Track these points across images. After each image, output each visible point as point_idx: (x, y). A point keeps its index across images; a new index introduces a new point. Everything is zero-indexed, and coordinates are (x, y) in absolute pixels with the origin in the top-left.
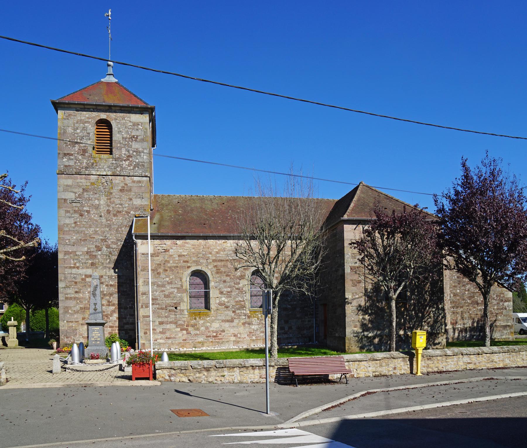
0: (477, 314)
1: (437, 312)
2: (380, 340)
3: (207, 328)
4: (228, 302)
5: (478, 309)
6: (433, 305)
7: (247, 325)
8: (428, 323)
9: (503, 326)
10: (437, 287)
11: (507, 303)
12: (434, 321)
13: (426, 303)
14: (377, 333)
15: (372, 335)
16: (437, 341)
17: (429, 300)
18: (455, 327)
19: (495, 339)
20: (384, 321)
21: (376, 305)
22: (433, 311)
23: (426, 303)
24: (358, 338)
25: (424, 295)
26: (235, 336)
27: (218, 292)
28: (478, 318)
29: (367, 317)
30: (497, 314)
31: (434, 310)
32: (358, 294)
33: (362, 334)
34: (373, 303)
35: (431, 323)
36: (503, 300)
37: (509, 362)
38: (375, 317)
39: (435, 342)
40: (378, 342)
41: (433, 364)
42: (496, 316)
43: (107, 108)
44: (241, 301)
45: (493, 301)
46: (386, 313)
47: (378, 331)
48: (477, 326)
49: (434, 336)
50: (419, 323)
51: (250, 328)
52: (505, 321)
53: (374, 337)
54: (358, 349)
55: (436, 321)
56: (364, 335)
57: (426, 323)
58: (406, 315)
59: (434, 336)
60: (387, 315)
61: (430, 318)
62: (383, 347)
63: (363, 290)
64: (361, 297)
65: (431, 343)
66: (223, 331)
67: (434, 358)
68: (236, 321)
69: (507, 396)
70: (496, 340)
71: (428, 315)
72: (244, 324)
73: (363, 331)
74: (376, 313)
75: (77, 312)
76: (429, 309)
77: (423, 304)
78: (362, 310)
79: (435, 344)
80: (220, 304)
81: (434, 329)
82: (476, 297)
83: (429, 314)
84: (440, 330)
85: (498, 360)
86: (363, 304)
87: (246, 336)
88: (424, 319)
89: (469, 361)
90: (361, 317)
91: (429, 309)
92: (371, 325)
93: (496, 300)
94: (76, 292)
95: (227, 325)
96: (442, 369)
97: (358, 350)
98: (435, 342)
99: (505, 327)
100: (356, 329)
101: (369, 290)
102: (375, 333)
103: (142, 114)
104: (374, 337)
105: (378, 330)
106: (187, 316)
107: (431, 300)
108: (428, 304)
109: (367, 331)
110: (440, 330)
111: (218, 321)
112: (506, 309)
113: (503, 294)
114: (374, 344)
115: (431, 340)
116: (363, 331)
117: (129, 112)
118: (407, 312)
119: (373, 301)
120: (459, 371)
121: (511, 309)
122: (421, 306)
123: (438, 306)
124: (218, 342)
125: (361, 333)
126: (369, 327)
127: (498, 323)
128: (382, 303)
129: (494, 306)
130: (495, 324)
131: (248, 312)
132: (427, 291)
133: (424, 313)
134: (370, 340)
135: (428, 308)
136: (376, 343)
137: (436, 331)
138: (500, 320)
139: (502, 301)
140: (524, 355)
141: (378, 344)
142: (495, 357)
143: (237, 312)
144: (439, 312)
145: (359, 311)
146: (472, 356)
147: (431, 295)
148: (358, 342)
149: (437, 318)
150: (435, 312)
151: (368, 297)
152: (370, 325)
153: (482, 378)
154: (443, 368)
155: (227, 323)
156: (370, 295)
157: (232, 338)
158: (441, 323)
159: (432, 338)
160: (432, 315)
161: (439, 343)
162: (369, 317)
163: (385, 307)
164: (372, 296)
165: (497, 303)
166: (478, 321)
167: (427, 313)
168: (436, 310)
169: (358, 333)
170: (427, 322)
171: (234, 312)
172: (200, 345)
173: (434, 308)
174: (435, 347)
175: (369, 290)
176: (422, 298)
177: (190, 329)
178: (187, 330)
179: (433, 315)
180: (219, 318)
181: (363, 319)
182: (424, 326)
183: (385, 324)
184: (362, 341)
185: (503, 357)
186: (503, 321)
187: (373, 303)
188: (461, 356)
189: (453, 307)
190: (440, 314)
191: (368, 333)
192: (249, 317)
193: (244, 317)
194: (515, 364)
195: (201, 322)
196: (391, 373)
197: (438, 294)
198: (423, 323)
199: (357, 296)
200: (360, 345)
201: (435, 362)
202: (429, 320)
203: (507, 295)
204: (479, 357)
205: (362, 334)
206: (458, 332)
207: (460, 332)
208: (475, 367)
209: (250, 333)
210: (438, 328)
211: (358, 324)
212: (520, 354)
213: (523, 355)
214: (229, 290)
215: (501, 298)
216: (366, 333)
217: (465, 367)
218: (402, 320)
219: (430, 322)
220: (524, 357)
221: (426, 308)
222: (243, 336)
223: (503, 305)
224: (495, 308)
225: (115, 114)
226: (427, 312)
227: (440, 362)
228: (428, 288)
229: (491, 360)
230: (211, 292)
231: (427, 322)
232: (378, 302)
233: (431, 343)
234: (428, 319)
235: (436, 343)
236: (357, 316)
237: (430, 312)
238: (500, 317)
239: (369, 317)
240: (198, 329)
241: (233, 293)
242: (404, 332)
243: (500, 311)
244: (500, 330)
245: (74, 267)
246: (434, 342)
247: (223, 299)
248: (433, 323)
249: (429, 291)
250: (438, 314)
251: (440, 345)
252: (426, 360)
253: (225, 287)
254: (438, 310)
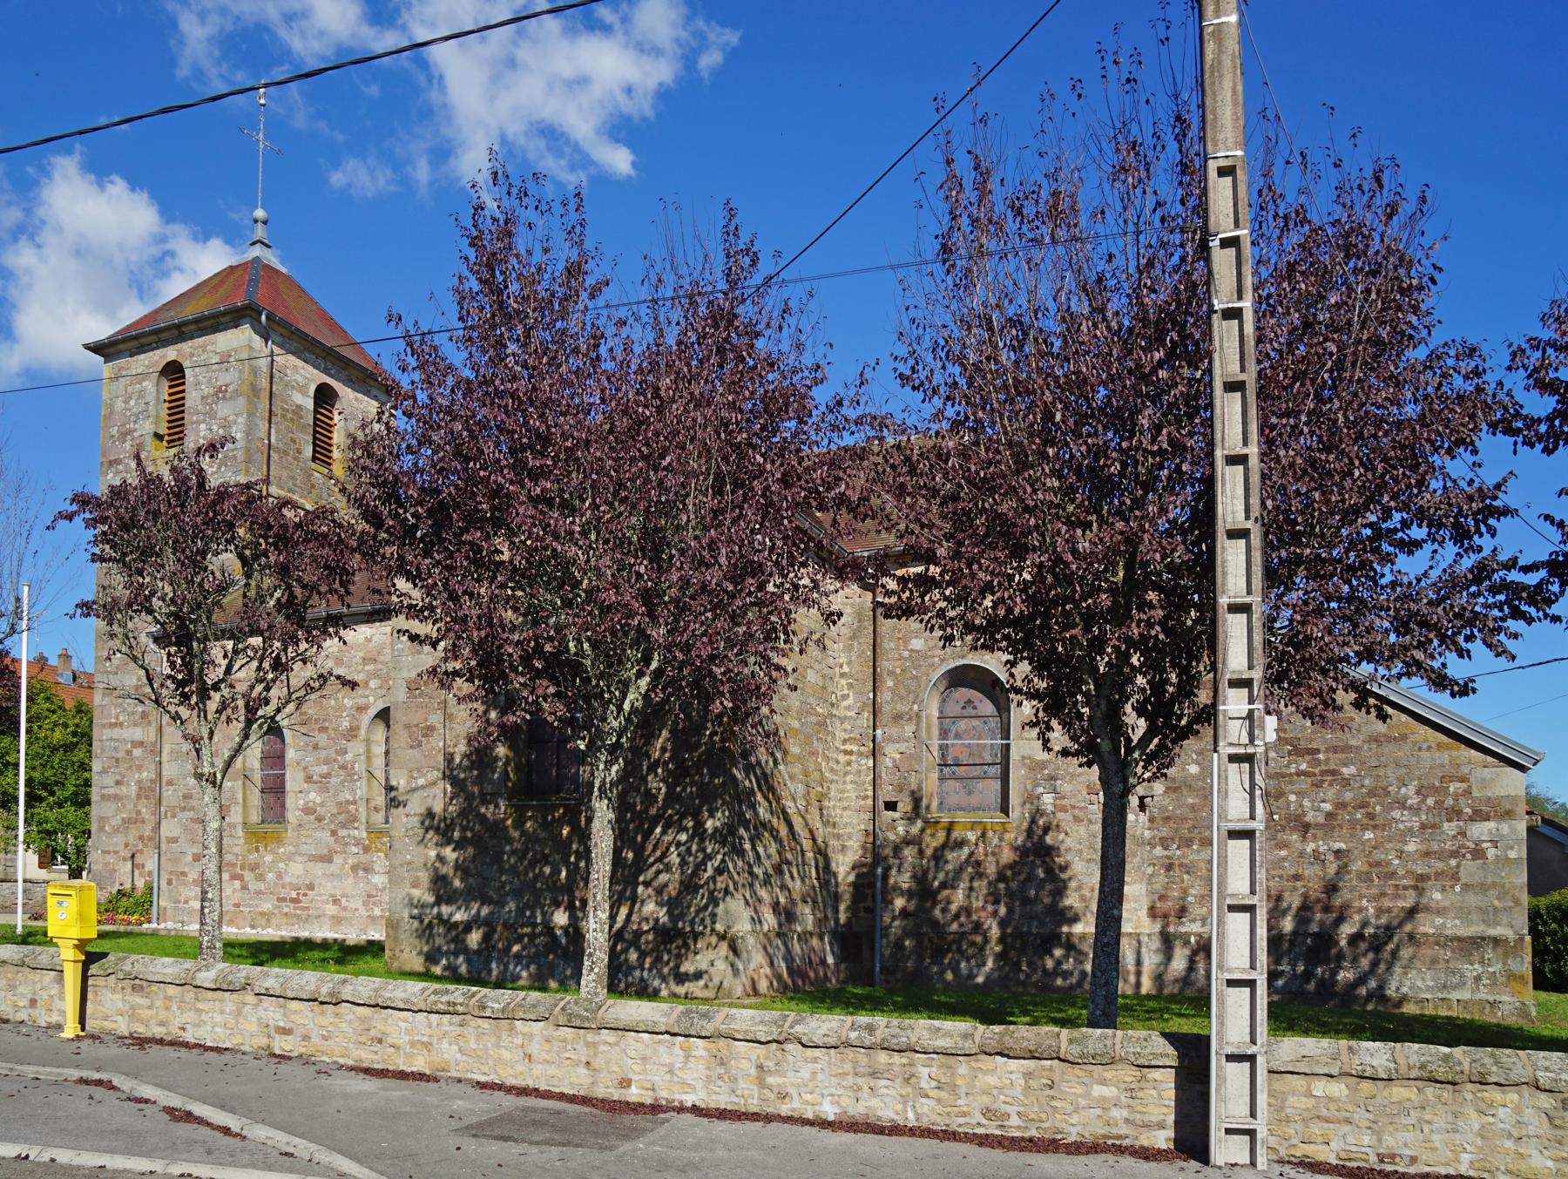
0: (1296, 877)
1: (694, 848)
2: (487, 938)
3: (280, 876)
4: (322, 805)
5: (1302, 854)
6: (680, 820)
7: (361, 873)
8: (659, 891)
9: (1459, 939)
10: (698, 745)
11: (1492, 825)
12: (681, 882)
13: (653, 811)
14: (479, 911)
15: (465, 917)
16: (687, 967)
17: (664, 800)
18: (1171, 929)
19: (1403, 999)
20: (502, 871)
21: (479, 814)
22: (679, 844)
23: (653, 811)
24: (422, 922)
25: (644, 780)
26: (336, 902)
27: (302, 774)
28: (1305, 896)
29: (449, 853)
30: (1422, 878)
31: (683, 837)
32: (424, 775)
33: (435, 910)
34: (470, 805)
35: (673, 890)
36: (1459, 813)
37: (458, 1056)
38: (474, 857)
39: (683, 969)
40: (479, 944)
41: (150, 1007)
42: (1415, 888)
43: (176, 332)
44: (348, 802)
45: (1396, 814)
46: (510, 841)
47: (482, 904)
48: (1295, 933)
49: (680, 942)
50: (625, 890)
51: (369, 882)
52: (1474, 917)
53: (468, 927)
54: (421, 960)
55: (689, 886)
56: (439, 916)
57: (650, 890)
58: (577, 852)
59: (680, 942)
60: (514, 852)
61: (668, 868)
62: (494, 965)
63: (441, 758)
64: (435, 784)
65: (666, 970)
66: (311, 887)
67: (154, 987)
68: (338, 859)
69: (90, 1160)
70: (1409, 1009)
71: (659, 860)
72: (355, 868)
73: (438, 902)
74: (476, 842)
75: (117, 830)
76: (664, 833)
77: (640, 813)
78: (437, 830)
79: (681, 978)
80: (308, 811)
81: (681, 916)
82: (1293, 798)
83: (665, 854)
84: (708, 921)
85: (407, 1038)
86: (438, 808)
87: (359, 904)
88: (641, 871)
89: (281, 1024)
90: (433, 853)
91: (664, 833)
92: (462, 880)
93: (1415, 810)
94: (118, 783)
95: (318, 869)
96: (180, 1033)
97: (418, 964)
98: (683, 969)
99: (1471, 945)
100: (416, 893)
101: (457, 760)
102: (473, 912)
103: (236, 327)
104: (468, 927)
105: (485, 900)
106: (242, 841)
107: (671, 798)
108: (662, 816)
109: (449, 902)
110: (708, 921)
111: (300, 859)
112: (1478, 853)
113: (1462, 780)
114: (465, 950)
115: (666, 958)
116: (438, 902)
117: (216, 329)
118: (580, 843)
119: (470, 798)
120: (290, 1058)
121: (1513, 854)
122: (632, 820)
123: (699, 825)
124: (298, 917)
125: (433, 906)
126: (455, 891)
127: (1426, 925)
128: (497, 806)
129: (1405, 843)
130: (1408, 928)
131: (364, 834)
132: (657, 763)
133: (642, 847)
134: (458, 932)
135: (658, 830)
136: (475, 947)
137: (692, 923)
138: (1440, 912)
139: (1455, 813)
140: (536, 1039)
141: (478, 952)
142: (397, 1026)
143: (342, 833)
144: (703, 850)
145: (427, 830)
146: (295, 1005)
147: (677, 776)
148: (419, 937)
149: (695, 874)
150: (689, 850)
151: (454, 781)
152: (457, 883)
153: (75, 1074)
154: (183, 1029)
155: (320, 865)
156: (462, 776)
157: (331, 909)
158: (711, 893)
159: (669, 952)
160: (674, 858)
161: (698, 975)
162: (455, 855)
163: (505, 820)
164: (465, 780)
165: (1423, 827)
166: (1305, 907)
167: (654, 851)
168: (691, 839)
169: (423, 906)
170: (656, 884)
171: (334, 833)
172: (263, 922)
173: (686, 829)
174: (681, 990)
175: (457, 760)
176: (637, 790)
177: (248, 876)
178: (240, 877)
179: (678, 860)
180: (304, 849)
181: (440, 858)
182: (643, 902)
183: (504, 884)
184: (431, 935)
185: (428, 1031)
186: (1463, 913)
187: (470, 805)
188: (250, 998)
189: (1164, 843)
190: (709, 857)
191: (454, 907)
192: (366, 850)
193: (355, 850)
194: (485, 1069)
195: (268, 858)
196: (22, 1016)
197: (702, 775)
198: (640, 889)
199: (421, 782)
200: (426, 949)
201: (159, 1003)
202: (664, 877)
203: (1485, 783)
204: (323, 1013)
205: (435, 910)
206: (1187, 952)
207: (1194, 953)
208: (303, 1050)
209: (369, 896)
210: (697, 912)
211: (425, 877)
212: (512, 1029)
213: (530, 1036)
214: (325, 769)
215: (1450, 802)
216: (446, 910)
217: (264, 1041)
218: (564, 874)
219: (666, 885)
220: (535, 1048)
221: (651, 831)
222: (353, 906)
223: (1463, 834)
224: (1411, 847)
225: (190, 343)
226: (655, 847)
227: (174, 1008)
228: (664, 750)
229: (373, 1033)
230: (288, 777)
231: (656, 884)
232: (485, 802)
233: (666, 970)
234: (658, 872)
235: (686, 974)
236: (421, 848)
237: (668, 849)
238: (1437, 896)
239: (455, 855)
240: (260, 878)
241: (333, 780)
242: (570, 917)
243: (1440, 865)
244: (1434, 961)
245: (115, 725)
246: (678, 966)
247: (313, 795)
248: (680, 893)
249: (666, 763)
250: (700, 855)
251: (701, 983)
252: (128, 990)
253: (318, 762)
254: (702, 840)
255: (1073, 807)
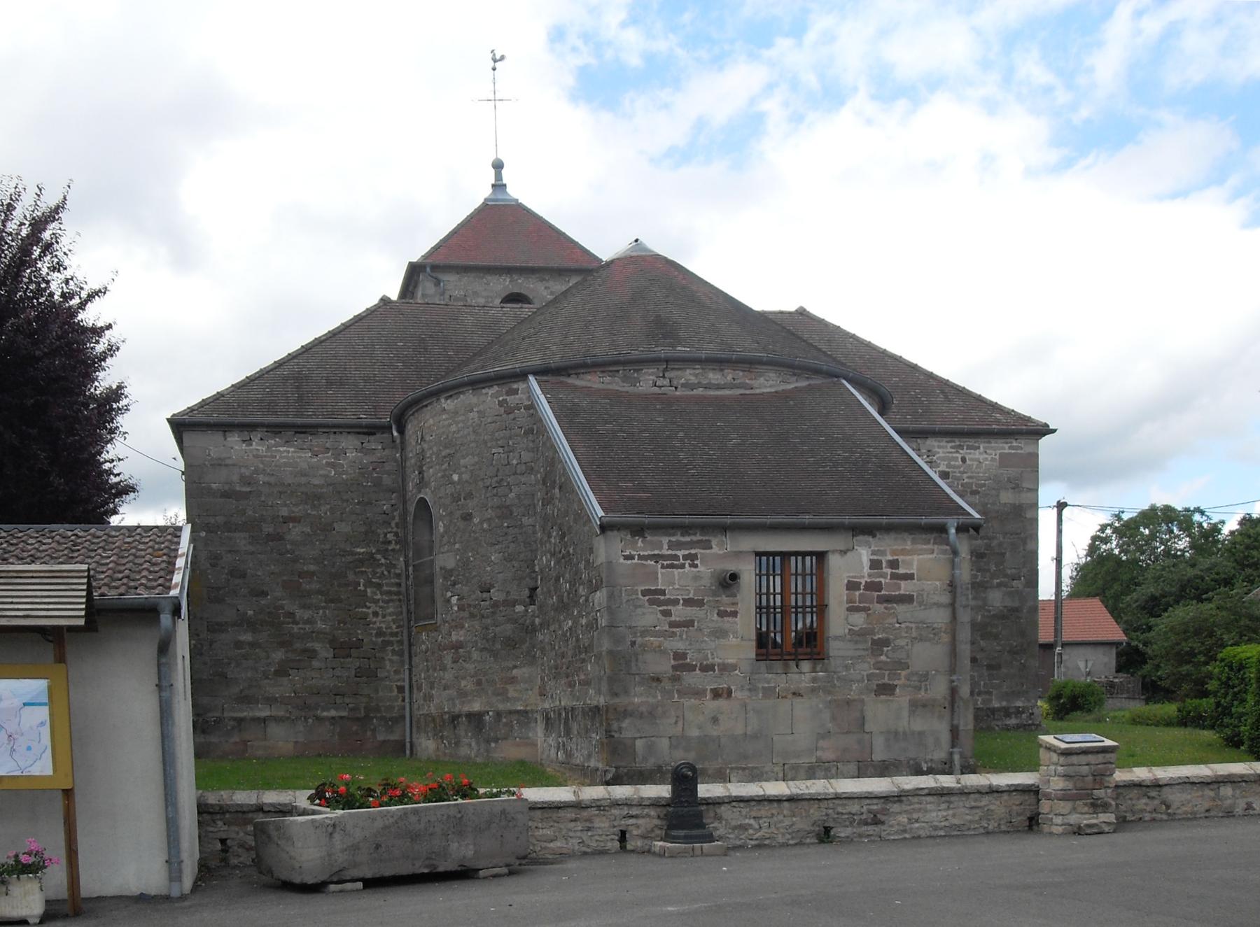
255: (469, 606)
